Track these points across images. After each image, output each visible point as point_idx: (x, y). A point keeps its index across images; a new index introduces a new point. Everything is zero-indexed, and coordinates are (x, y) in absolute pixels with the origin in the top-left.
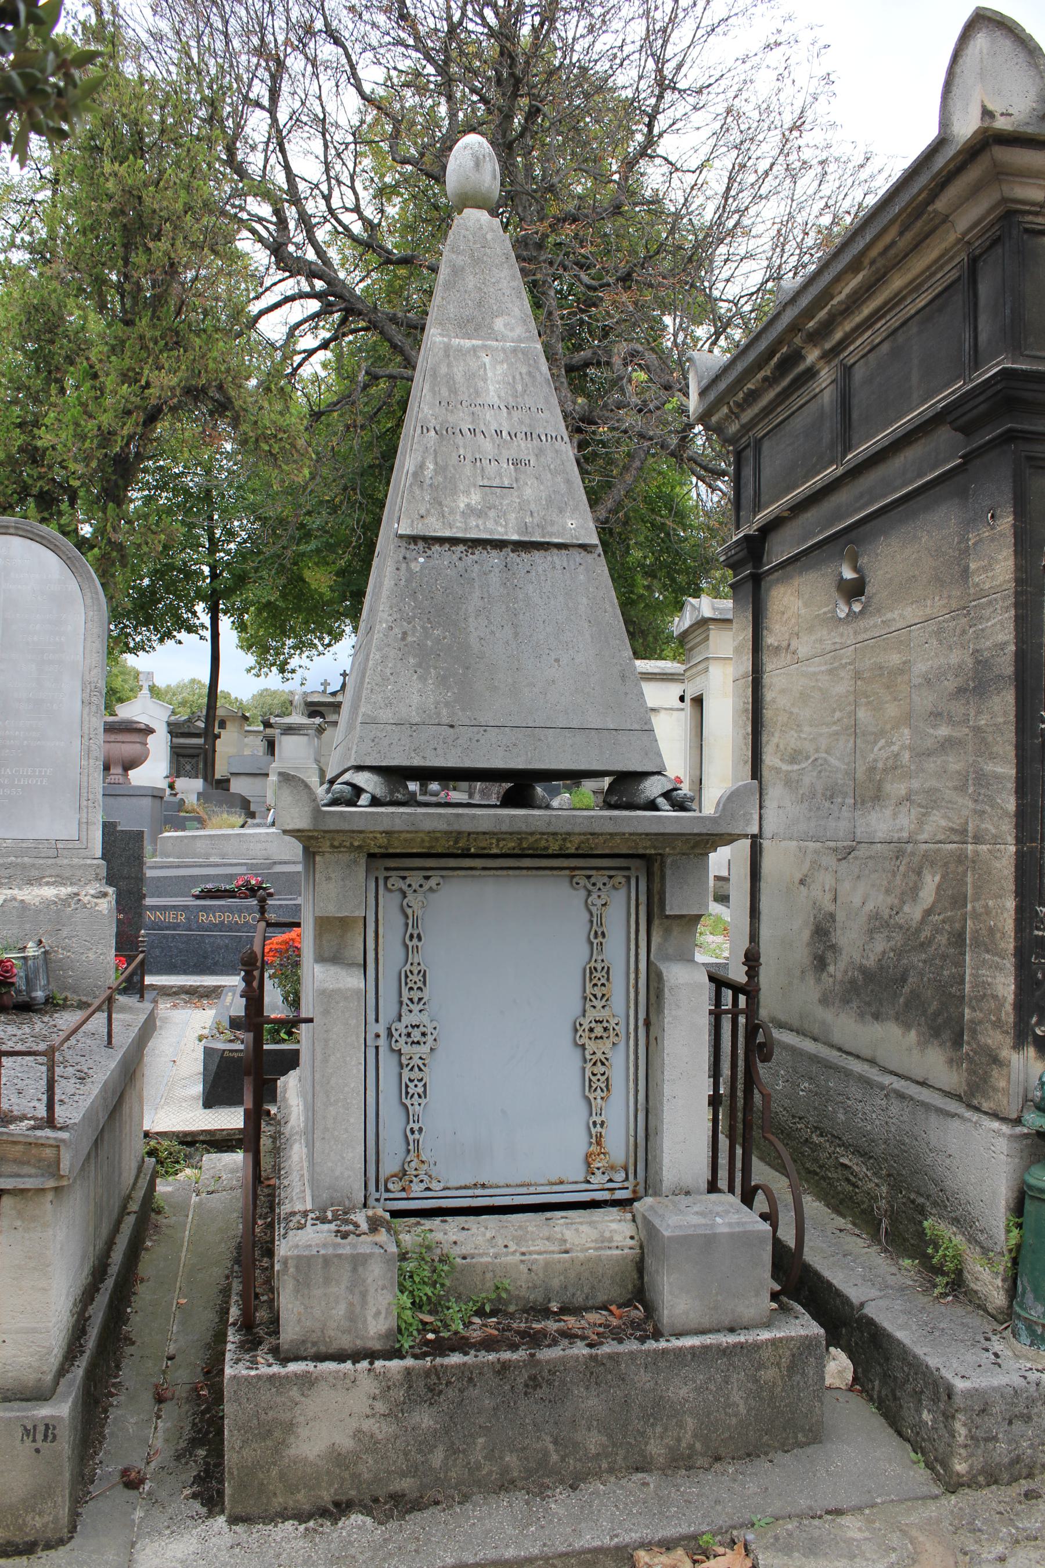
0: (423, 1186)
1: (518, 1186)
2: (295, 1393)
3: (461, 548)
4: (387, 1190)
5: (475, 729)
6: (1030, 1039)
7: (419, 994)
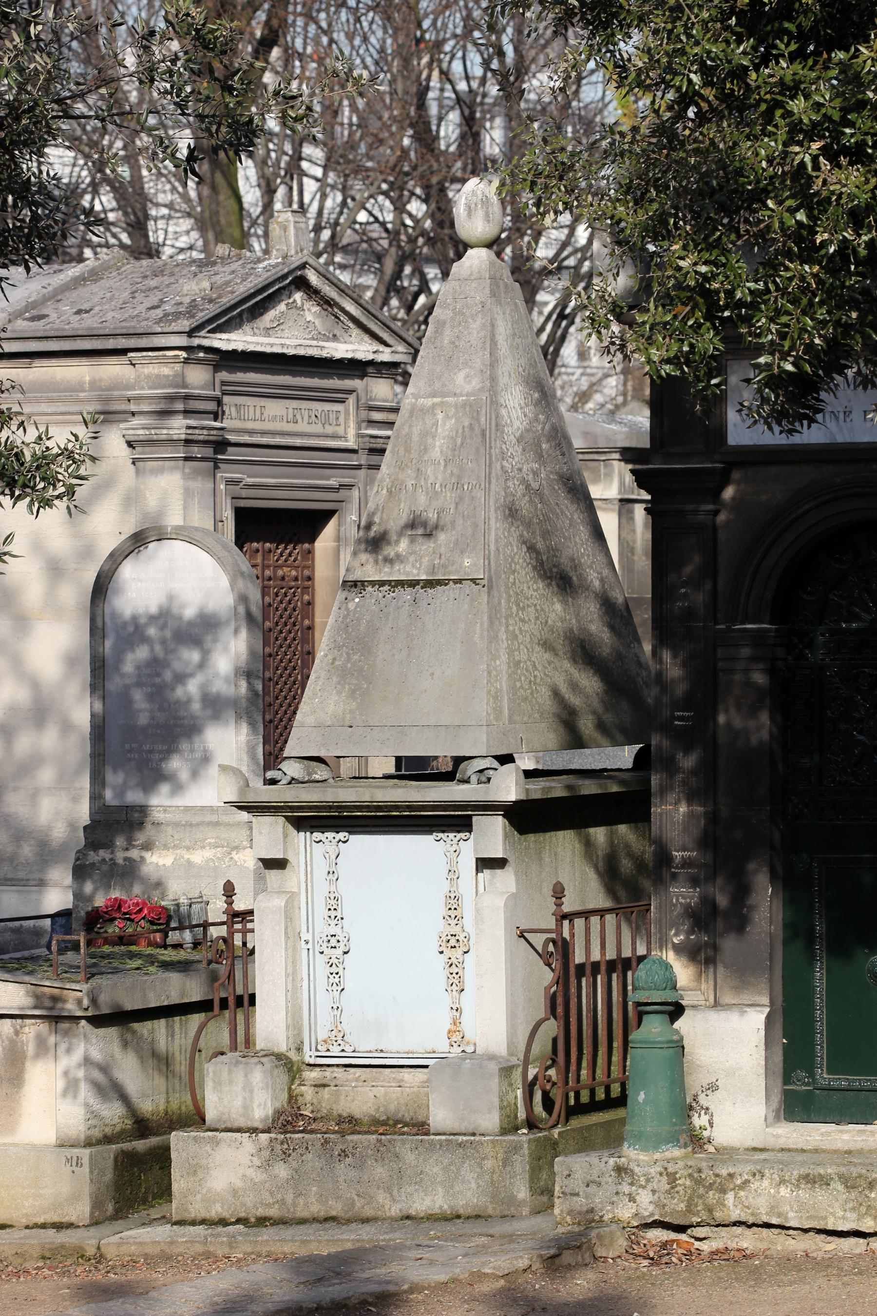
0: (340, 1048)
3: (387, 588)
4: (317, 1050)
6: (670, 946)
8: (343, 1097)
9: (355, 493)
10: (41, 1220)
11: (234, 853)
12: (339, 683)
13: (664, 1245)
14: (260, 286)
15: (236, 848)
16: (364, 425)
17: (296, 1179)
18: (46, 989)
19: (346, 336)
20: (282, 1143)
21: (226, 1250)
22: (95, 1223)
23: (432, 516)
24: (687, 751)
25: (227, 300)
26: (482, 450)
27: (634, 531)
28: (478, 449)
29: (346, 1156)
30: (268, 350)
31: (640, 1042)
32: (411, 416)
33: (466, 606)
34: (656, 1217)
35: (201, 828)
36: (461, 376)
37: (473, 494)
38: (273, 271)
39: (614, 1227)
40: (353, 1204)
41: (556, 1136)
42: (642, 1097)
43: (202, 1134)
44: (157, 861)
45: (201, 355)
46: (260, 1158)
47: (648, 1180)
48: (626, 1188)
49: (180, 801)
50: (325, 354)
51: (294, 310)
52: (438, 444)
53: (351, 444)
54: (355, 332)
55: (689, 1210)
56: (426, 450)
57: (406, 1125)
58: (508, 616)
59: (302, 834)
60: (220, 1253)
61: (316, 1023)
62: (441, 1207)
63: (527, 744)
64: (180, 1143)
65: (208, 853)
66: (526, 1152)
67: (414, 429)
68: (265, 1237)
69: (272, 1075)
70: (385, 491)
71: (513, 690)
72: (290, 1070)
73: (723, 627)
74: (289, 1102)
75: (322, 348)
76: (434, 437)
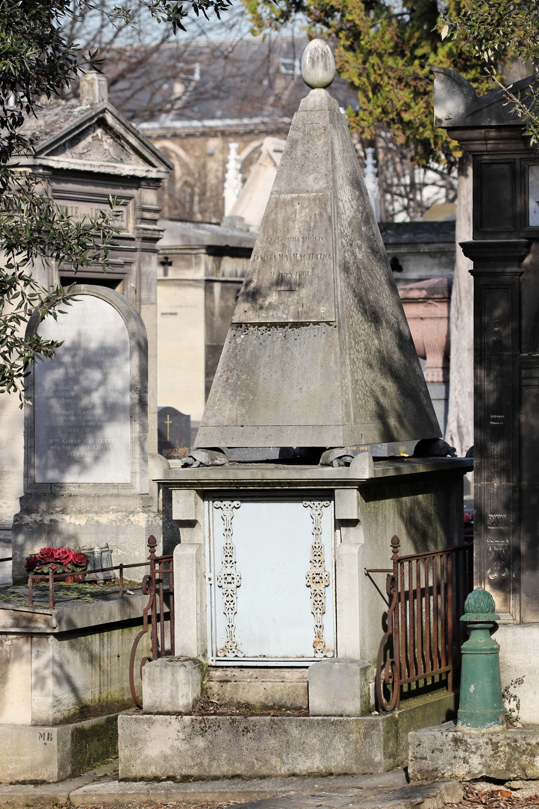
0: (234, 655)
1: (284, 658)
2: (146, 726)
3: (264, 328)
4: (217, 656)
5: (253, 428)
6: (487, 581)
7: (319, 558)
8: (241, 689)
9: (134, 268)
10: (21, 778)
11: (131, 516)
12: (232, 395)
13: (492, 794)
14: (78, 124)
15: (132, 512)
16: (139, 221)
17: (211, 748)
18: (24, 614)
19: (128, 159)
20: (200, 723)
21: (164, 800)
22: (61, 780)
23: (295, 277)
24: (496, 441)
25: (58, 133)
26: (330, 231)
27: (213, 301)
28: (326, 230)
29: (248, 731)
30: (82, 168)
31: (471, 650)
32: (276, 207)
33: (323, 341)
34: (484, 774)
35: (106, 498)
36: (311, 178)
37: (325, 262)
38: (86, 114)
39: (455, 782)
40: (253, 766)
41: (397, 716)
42: (472, 689)
43: (141, 717)
44: (70, 522)
45: (41, 171)
46: (184, 733)
47: (478, 748)
48: (461, 754)
49: (84, 479)
50: (116, 172)
51: (96, 142)
52: (297, 226)
53: (131, 234)
54: (134, 157)
55: (508, 769)
56: (288, 230)
57: (288, 709)
58: (350, 348)
59: (206, 503)
60: (159, 801)
61: (216, 637)
62: (318, 768)
63: (365, 438)
64: (125, 722)
65: (112, 516)
66: (381, 728)
67: (279, 216)
68: (193, 790)
69: (192, 673)
70: (259, 260)
71: (355, 400)
72: (202, 670)
73: (525, 355)
74: (202, 694)
75: (115, 167)
76: (294, 222)
